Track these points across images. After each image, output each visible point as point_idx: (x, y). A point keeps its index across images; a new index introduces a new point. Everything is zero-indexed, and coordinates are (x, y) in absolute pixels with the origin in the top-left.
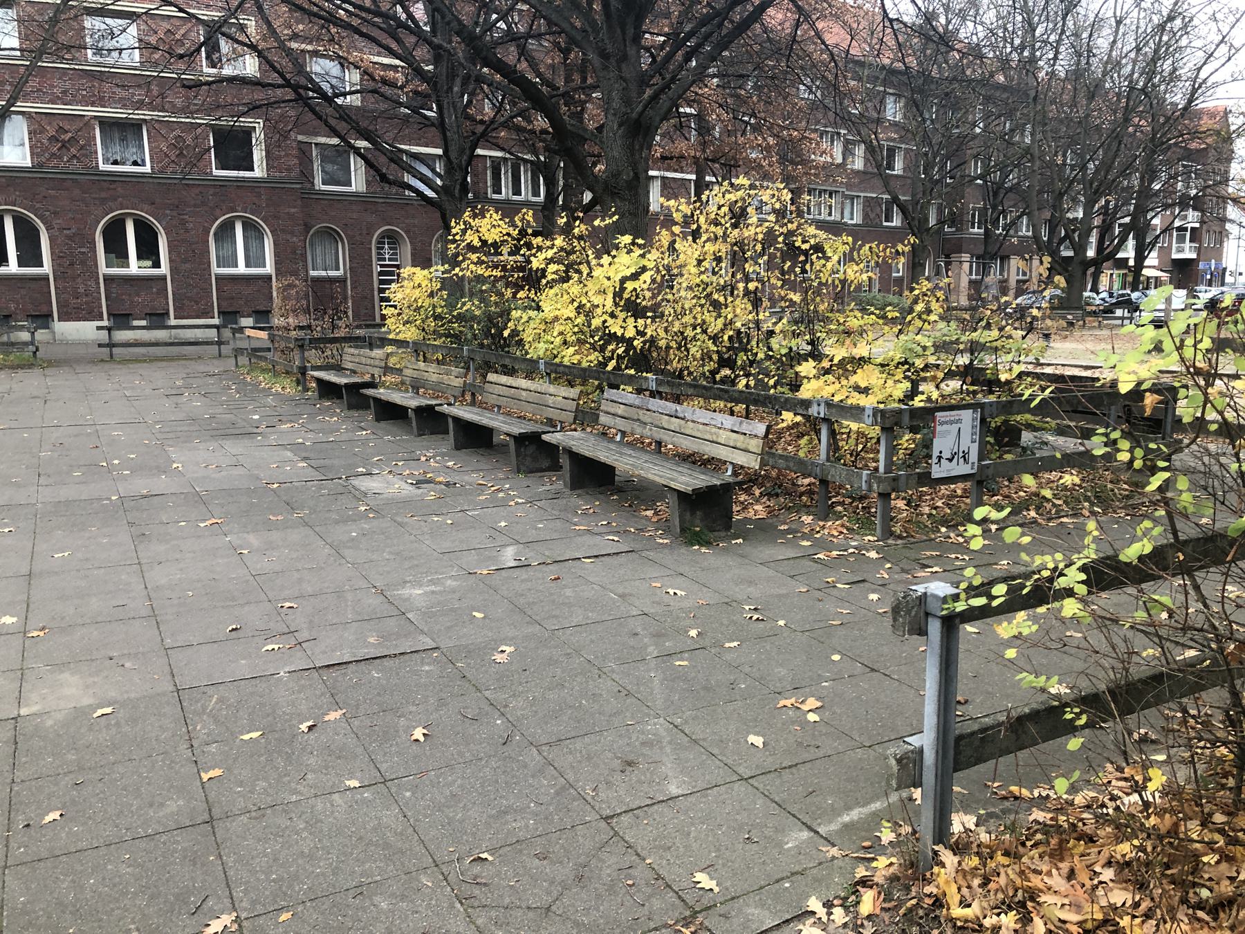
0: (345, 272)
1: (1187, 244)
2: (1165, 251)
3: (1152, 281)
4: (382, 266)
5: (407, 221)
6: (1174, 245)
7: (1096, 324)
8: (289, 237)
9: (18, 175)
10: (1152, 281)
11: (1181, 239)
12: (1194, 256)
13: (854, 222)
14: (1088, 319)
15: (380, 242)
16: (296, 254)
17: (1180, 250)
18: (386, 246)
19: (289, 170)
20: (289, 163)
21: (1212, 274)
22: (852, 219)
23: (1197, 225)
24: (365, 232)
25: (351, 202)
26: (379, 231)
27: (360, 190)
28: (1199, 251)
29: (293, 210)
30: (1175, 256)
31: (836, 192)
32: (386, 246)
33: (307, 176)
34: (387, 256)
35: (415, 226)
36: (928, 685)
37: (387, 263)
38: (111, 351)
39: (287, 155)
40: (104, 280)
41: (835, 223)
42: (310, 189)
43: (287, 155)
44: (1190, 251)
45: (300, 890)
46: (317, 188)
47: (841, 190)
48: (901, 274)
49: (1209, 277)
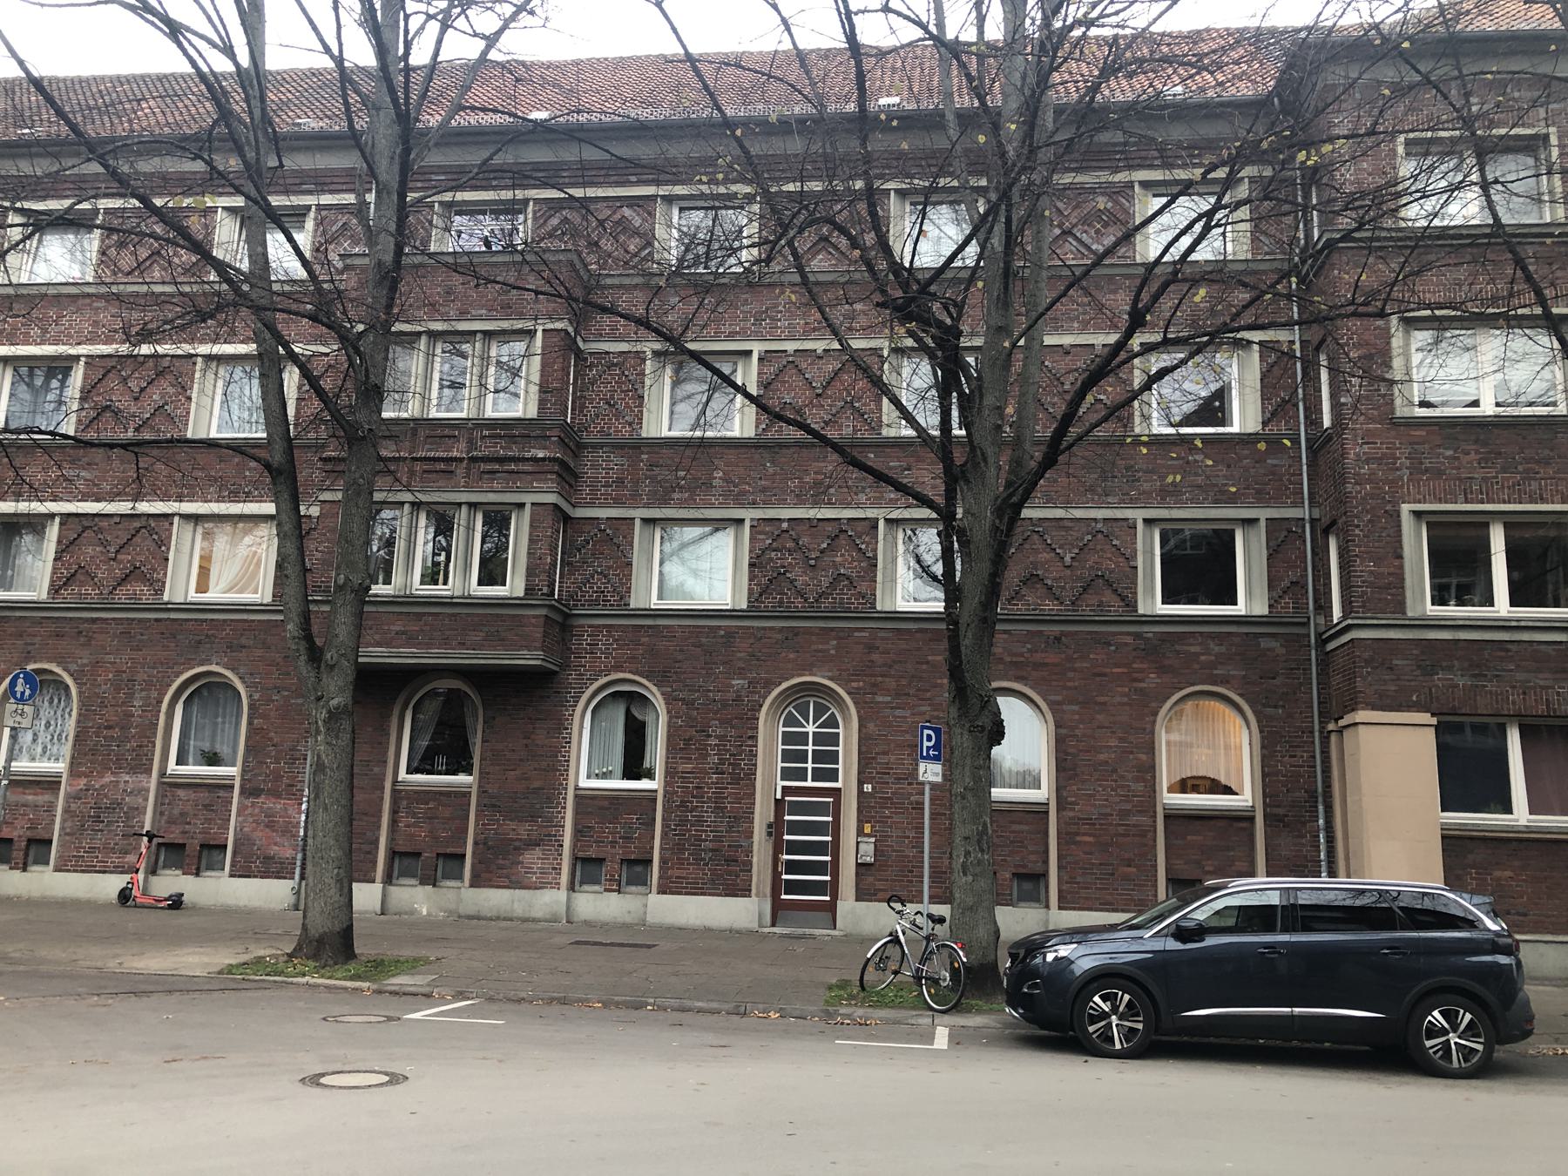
40: (1166, 817)
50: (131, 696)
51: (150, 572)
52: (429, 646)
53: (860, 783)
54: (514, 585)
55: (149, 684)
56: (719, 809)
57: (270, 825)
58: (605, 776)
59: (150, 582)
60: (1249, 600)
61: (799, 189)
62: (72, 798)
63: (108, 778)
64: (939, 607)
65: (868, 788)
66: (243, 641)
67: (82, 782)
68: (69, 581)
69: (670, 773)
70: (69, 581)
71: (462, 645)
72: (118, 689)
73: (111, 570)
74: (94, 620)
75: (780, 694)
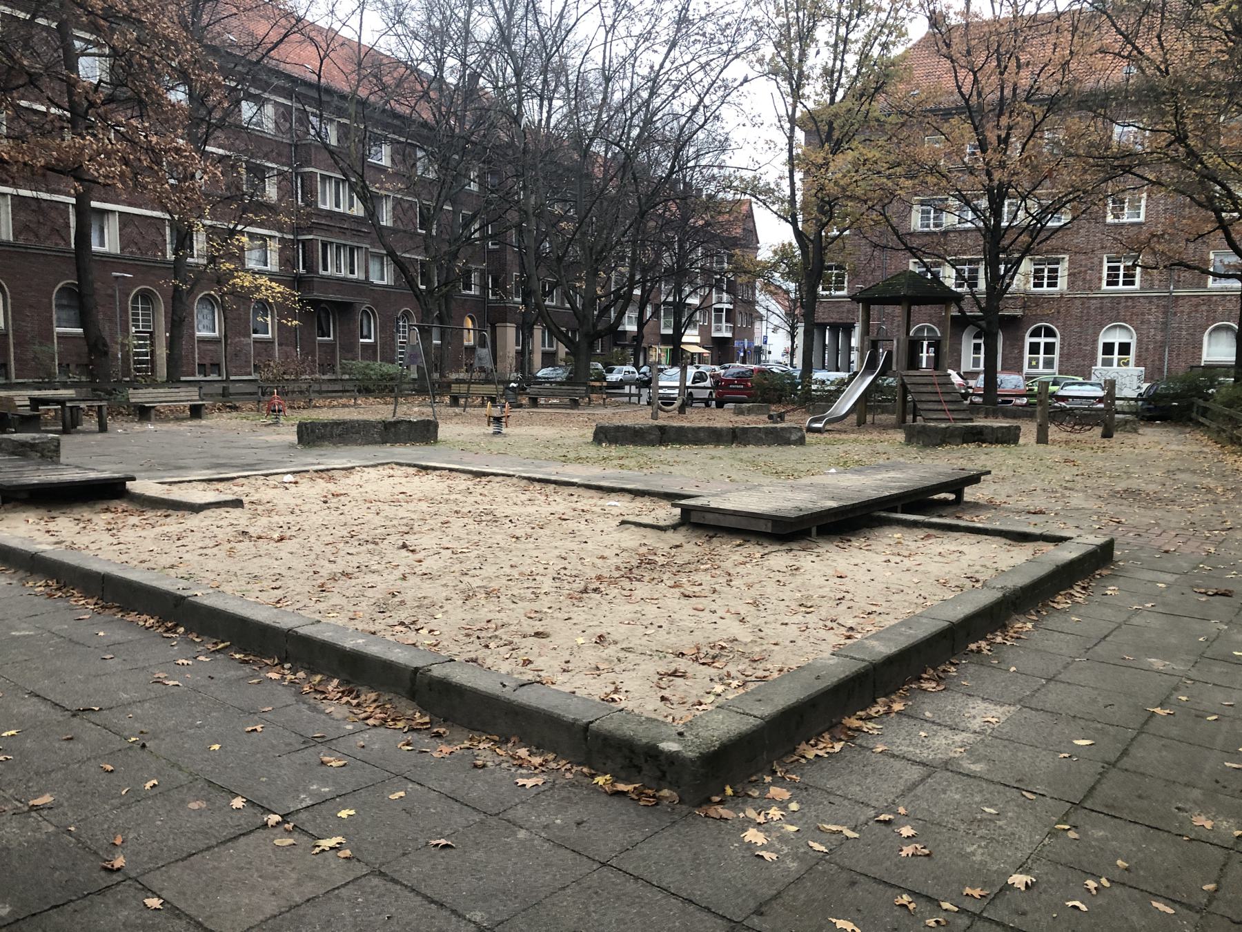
0: (273, 338)
1: (724, 324)
2: (704, 331)
3: (696, 356)
6: (713, 324)
7: (601, 402)
10: (696, 356)
11: (718, 320)
12: (729, 335)
13: (385, 283)
14: (593, 396)
15: (135, 301)
17: (719, 330)
21: (745, 352)
22: (382, 279)
23: (731, 307)
26: (60, 285)
27: (113, 251)
28: (733, 330)
30: (715, 334)
31: (358, 247)
36: (989, 424)
38: (469, 387)
40: (58, 337)
41: (357, 281)
44: (726, 330)
45: (111, 921)
47: (364, 246)
49: (742, 354)
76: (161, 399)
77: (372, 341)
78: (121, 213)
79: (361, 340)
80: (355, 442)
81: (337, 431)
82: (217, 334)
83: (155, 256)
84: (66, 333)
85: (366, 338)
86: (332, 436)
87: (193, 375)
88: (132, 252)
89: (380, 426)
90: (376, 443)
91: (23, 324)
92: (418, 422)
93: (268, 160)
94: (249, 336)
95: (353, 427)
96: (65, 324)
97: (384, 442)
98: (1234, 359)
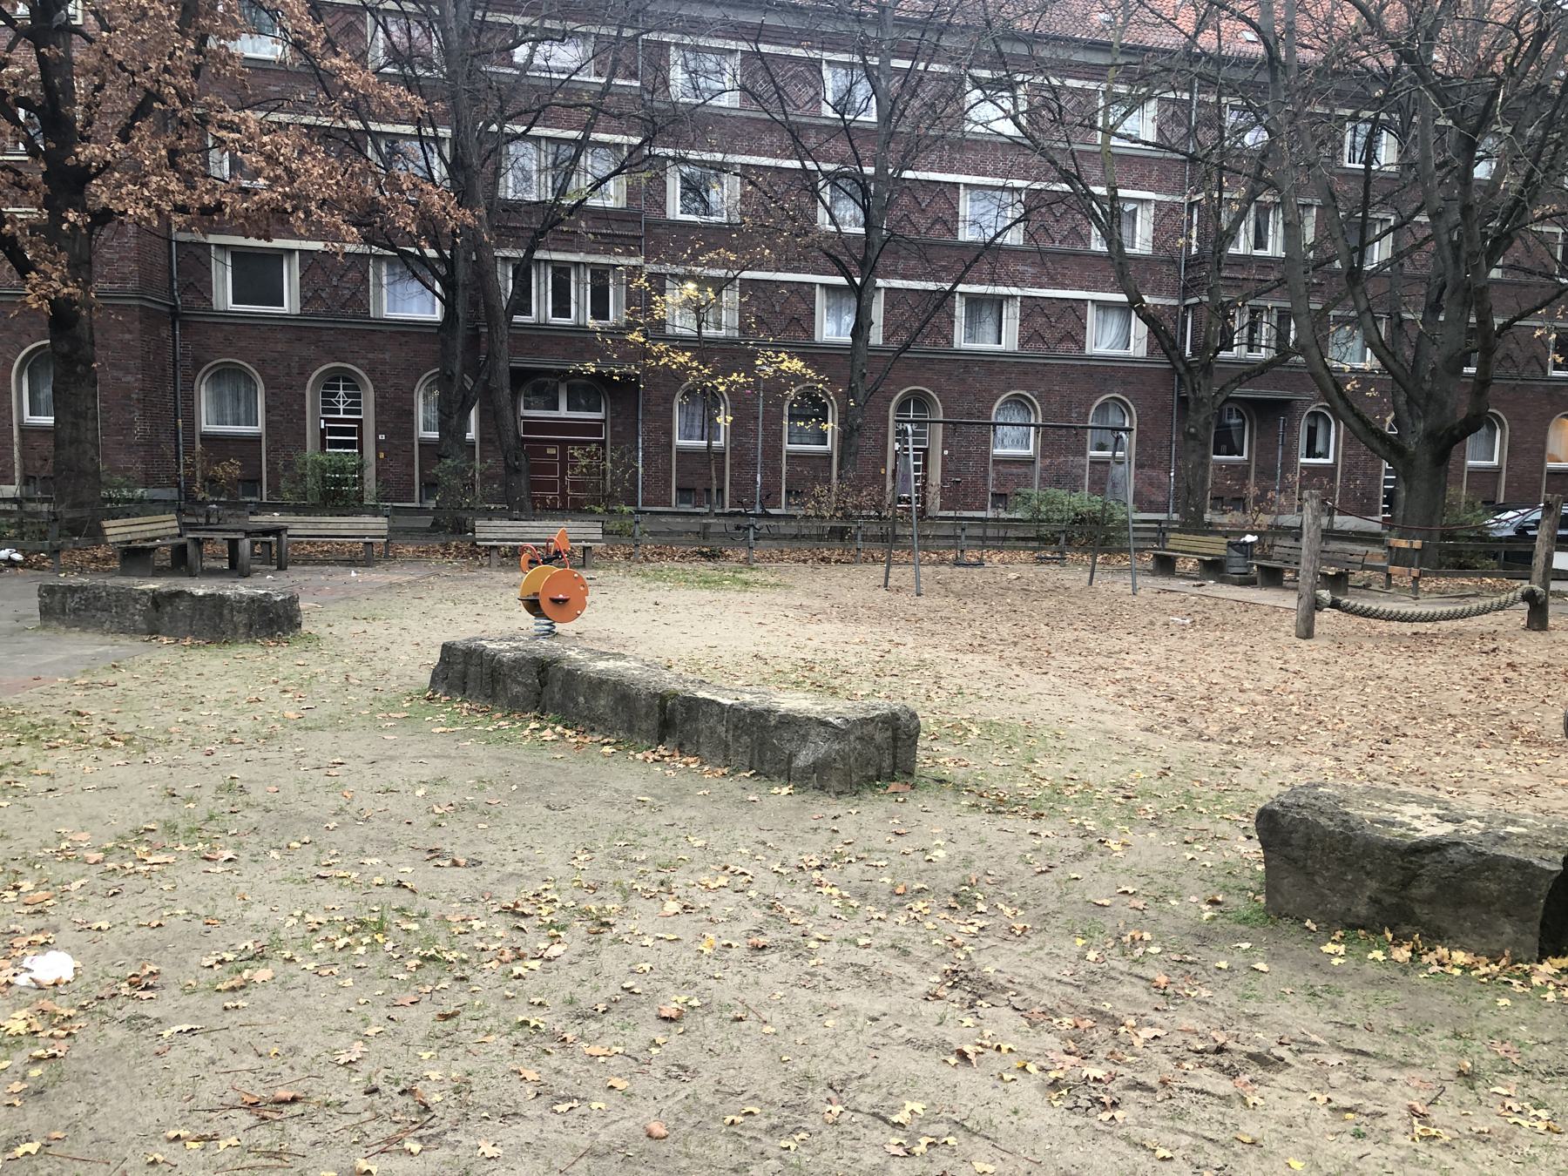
4: (327, 420)
5: (370, 356)
8: (120, 374)
9: (565, 334)
15: (903, 407)
16: (130, 399)
18: (341, 392)
19: (124, 280)
20: (126, 270)
24: (295, 371)
25: (272, 329)
29: (127, 336)
32: (341, 392)
33: (201, 288)
34: (341, 407)
35: (384, 363)
37: (341, 416)
39: (122, 259)
40: (420, 445)
42: (204, 309)
43: (122, 259)
46: (956, 346)
48: (1496, 462)
50: (1070, 410)
51: (1076, 337)
52: (1259, 388)
53: (943, 450)
54: (1263, 354)
55: (1080, 405)
56: (1365, 474)
57: (1151, 484)
58: (690, 437)
59: (1076, 342)
60: (290, 303)
61: (489, 14)
62: (1045, 469)
63: (1062, 459)
64: (438, 316)
65: (946, 452)
66: (1130, 379)
67: (1048, 461)
68: (1029, 340)
69: (268, 424)
70: (1029, 340)
71: (1275, 388)
72: (1062, 407)
73: (1052, 333)
74: (1045, 364)
75: (23, 358)
76: (534, 536)
77: (1330, 461)
78: (302, 251)
79: (1215, 457)
80: (99, 626)
81: (71, 603)
82: (1031, 451)
83: (935, 344)
84: (1014, 456)
85: (1319, 455)
86: (63, 611)
87: (984, 508)
88: (1068, 350)
89: (145, 599)
90: (134, 631)
91: (744, 439)
92: (205, 596)
93: (734, 152)
94: (1084, 454)
95: (98, 598)
96: (808, 440)
97: (153, 631)
98: (1558, 868)
